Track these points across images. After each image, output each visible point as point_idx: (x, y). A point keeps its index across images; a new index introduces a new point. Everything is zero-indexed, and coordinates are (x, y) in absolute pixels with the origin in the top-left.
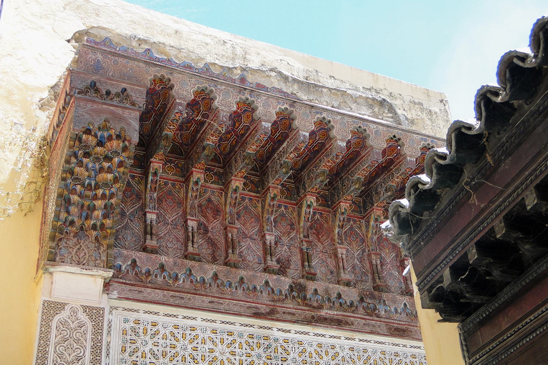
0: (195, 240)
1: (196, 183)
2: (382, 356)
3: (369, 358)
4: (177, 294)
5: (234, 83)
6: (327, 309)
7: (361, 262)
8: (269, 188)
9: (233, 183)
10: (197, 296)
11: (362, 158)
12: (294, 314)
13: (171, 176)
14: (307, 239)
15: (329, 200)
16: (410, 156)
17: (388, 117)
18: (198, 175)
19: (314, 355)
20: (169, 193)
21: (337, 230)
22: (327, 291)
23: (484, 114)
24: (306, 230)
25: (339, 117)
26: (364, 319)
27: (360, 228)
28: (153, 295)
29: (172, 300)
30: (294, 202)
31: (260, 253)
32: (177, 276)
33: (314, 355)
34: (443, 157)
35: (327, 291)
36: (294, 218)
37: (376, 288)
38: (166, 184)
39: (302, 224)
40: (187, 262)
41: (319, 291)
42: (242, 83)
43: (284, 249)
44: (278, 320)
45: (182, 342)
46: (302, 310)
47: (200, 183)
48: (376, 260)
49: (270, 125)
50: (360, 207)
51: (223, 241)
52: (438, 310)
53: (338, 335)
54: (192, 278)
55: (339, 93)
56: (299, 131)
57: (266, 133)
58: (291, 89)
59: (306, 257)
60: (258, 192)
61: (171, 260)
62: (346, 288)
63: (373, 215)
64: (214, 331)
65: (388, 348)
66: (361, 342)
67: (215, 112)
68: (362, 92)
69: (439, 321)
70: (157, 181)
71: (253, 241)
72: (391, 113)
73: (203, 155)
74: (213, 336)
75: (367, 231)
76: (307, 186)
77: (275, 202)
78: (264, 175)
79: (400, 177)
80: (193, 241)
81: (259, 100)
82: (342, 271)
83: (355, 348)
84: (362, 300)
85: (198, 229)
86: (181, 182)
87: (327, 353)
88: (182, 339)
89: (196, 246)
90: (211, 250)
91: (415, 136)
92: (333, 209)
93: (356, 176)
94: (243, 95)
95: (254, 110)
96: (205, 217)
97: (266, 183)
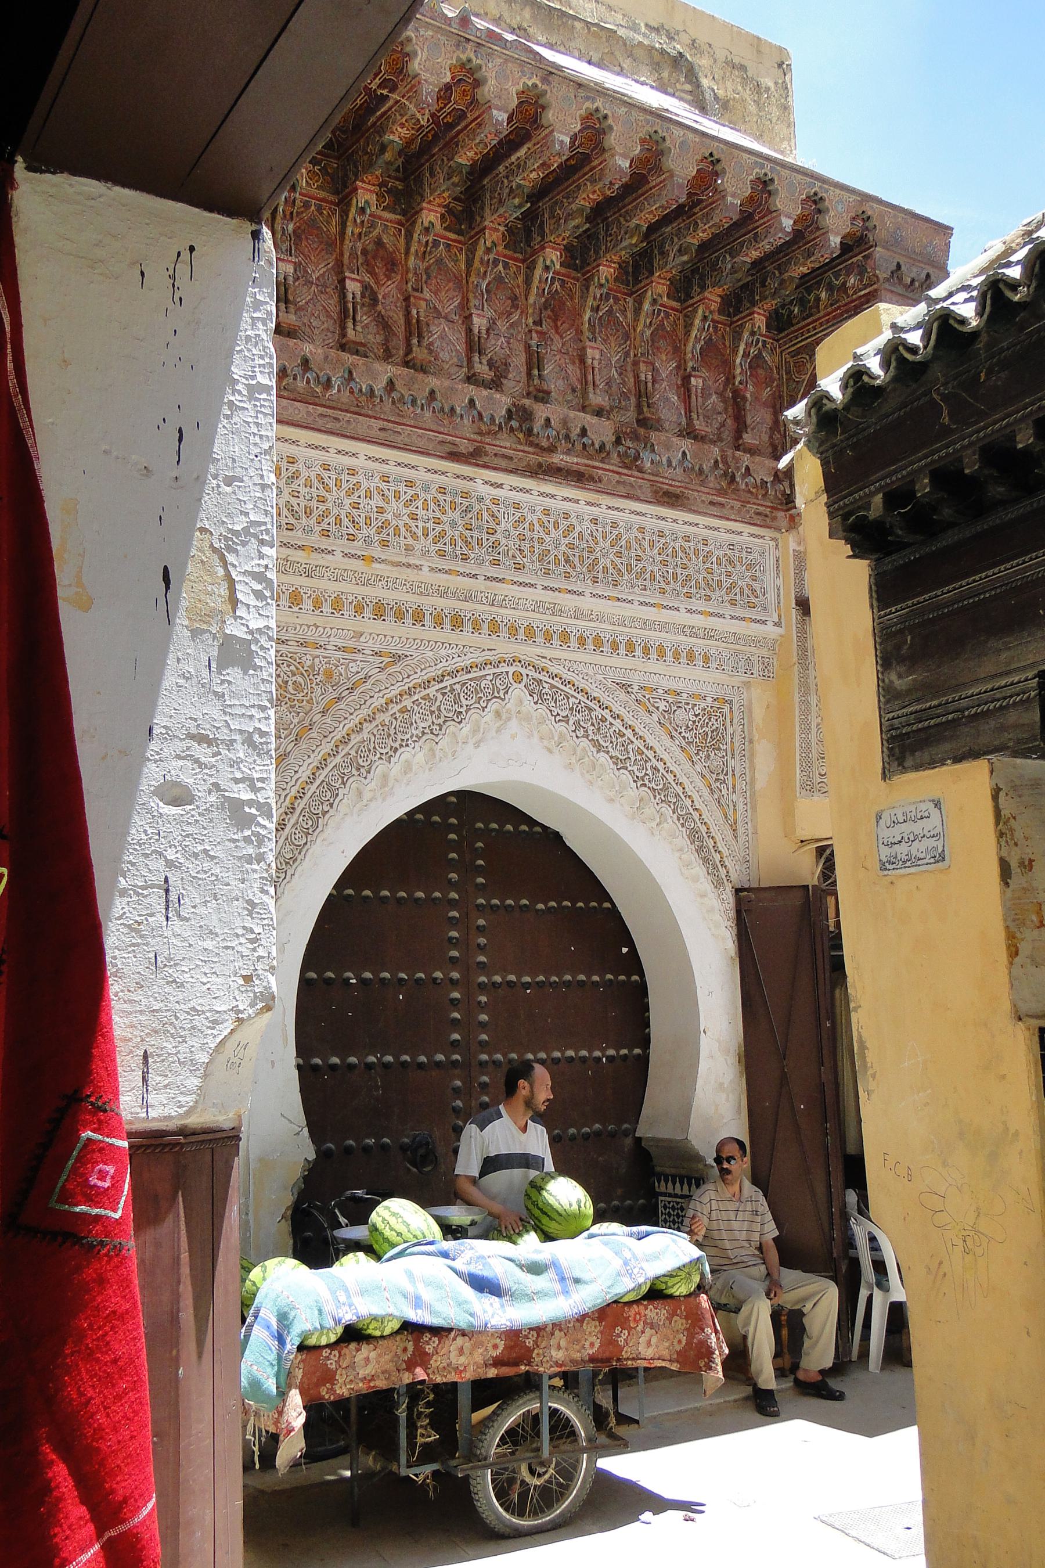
0: (358, 318)
1: (362, 211)
2: (640, 536)
3: (619, 537)
4: (330, 412)
5: (450, 25)
6: (563, 453)
7: (620, 374)
8: (484, 228)
9: (424, 216)
10: (360, 417)
11: (651, 189)
12: (511, 458)
13: (314, 191)
14: (539, 328)
15: (580, 257)
16: (733, 196)
17: (683, 91)
18: (366, 195)
19: (537, 527)
20: (312, 224)
21: (588, 315)
22: (565, 422)
23: (988, 309)
24: (537, 311)
25: (624, 109)
26: (618, 473)
27: (624, 312)
28: (291, 410)
29: (320, 422)
30: (520, 256)
31: (461, 348)
32: (329, 380)
33: (537, 527)
34: (913, 350)
35: (565, 422)
36: (519, 287)
37: (642, 422)
38: (306, 205)
39: (531, 300)
40: (345, 356)
41: (552, 421)
42: (462, 26)
43: (499, 343)
44: (485, 466)
45: (335, 493)
46: (524, 451)
47: (368, 212)
48: (646, 374)
49: (505, 116)
50: (627, 273)
51: (402, 322)
52: (848, 541)
53: (576, 498)
54: (352, 384)
55: (603, 34)
56: (552, 131)
57: (497, 133)
58: (518, 18)
59: (535, 360)
60: (460, 233)
61: (320, 351)
62: (595, 420)
63: (649, 293)
64: (385, 479)
65: (650, 523)
66: (609, 511)
67: (414, 83)
68: (644, 35)
69: (849, 557)
70: (294, 200)
71: (451, 325)
72: (690, 82)
73: (380, 161)
74: (383, 486)
75: (636, 320)
76: (547, 231)
77: (492, 256)
78: (475, 201)
79: (708, 230)
80: (354, 319)
81: (490, 65)
82: (591, 389)
83: (600, 520)
84: (618, 442)
85: (363, 296)
86: (331, 203)
87: (556, 525)
88: (335, 488)
89: (359, 328)
90: (382, 337)
91: (745, 156)
92: (583, 275)
93: (635, 221)
94: (463, 52)
95: (478, 83)
96: (373, 274)
97: (479, 219)
